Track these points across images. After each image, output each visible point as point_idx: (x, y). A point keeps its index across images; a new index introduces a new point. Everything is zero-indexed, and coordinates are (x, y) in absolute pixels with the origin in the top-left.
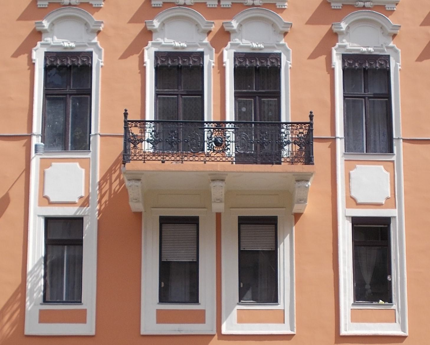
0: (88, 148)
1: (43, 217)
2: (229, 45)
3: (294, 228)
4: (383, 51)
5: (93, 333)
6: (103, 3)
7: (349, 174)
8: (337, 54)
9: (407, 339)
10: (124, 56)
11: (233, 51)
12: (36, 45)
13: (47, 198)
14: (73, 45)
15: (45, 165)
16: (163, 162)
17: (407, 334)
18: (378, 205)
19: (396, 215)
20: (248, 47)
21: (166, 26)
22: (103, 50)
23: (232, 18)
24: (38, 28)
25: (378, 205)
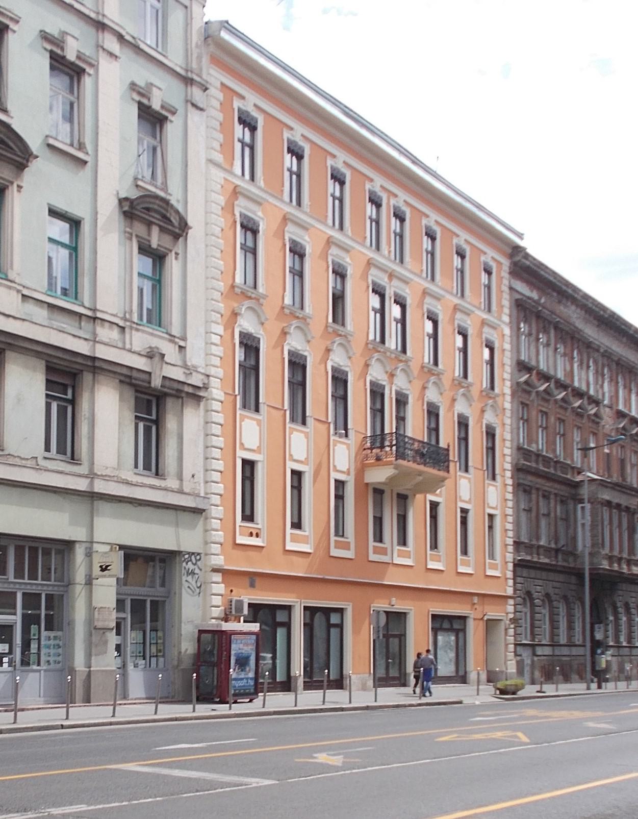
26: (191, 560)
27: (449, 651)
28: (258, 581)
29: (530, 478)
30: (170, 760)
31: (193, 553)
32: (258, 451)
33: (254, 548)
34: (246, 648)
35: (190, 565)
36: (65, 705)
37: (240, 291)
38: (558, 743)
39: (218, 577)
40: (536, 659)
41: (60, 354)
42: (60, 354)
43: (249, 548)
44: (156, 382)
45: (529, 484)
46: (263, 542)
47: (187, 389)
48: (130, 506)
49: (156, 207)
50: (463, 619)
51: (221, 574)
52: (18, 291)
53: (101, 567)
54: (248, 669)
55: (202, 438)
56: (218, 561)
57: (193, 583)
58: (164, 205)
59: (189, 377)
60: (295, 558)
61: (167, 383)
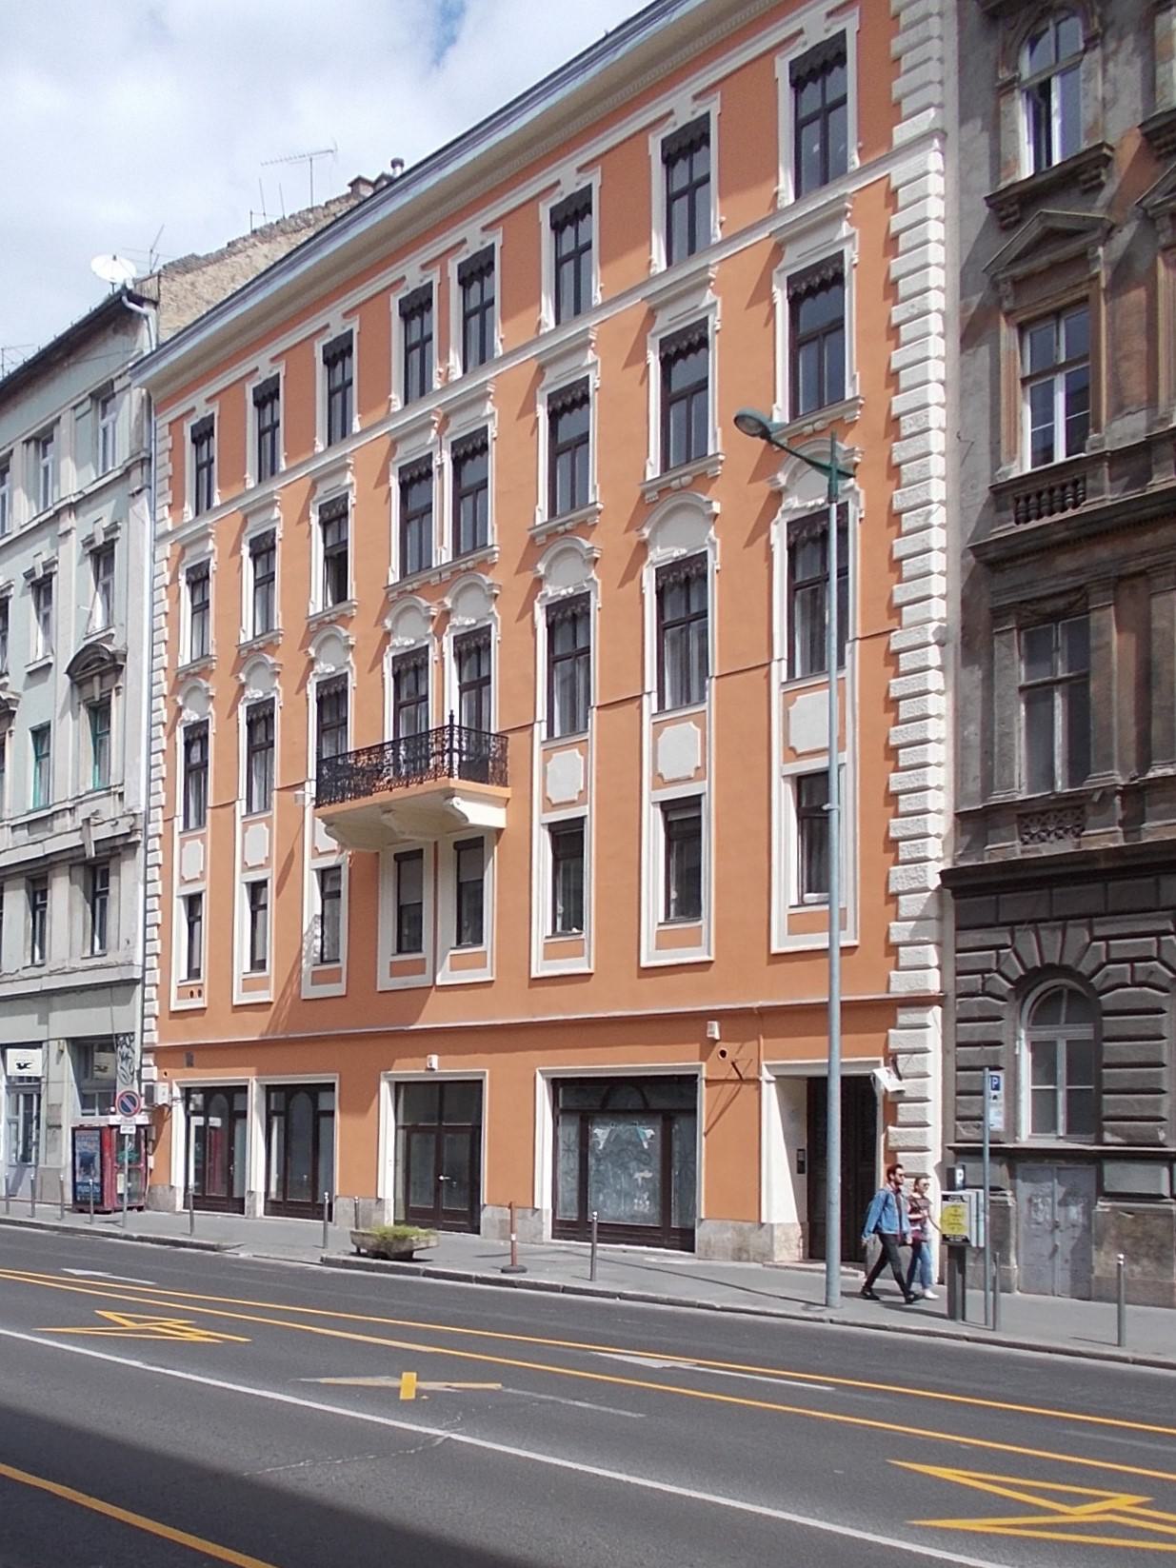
0: (76, 852)
1: (789, 779)
2: (448, 629)
3: (496, 848)
4: (583, 588)
5: (344, 993)
6: (859, 412)
7: (788, 713)
8: (541, 607)
9: (593, 977)
10: (622, 584)
11: (452, 635)
12: (775, 516)
13: (792, 749)
14: (684, 551)
15: (659, 728)
16: (421, 783)
17: (712, 958)
18: (572, 803)
19: (588, 813)
20: (804, 508)
21: (460, 600)
22: (862, 493)
23: (444, 596)
24: (776, 488)
25: (572, 803)
26: (125, 1043)
27: (633, 1164)
28: (197, 1057)
29: (1065, 562)
30: (1166, 1430)
31: (127, 1034)
32: (701, 772)
33: (784, 957)
34: (90, 1146)
35: (125, 1048)
36: (590, 1244)
37: (544, 537)
38: (323, 1380)
39: (149, 1060)
40: (1103, 1206)
41: (29, 867)
42: (29, 867)
43: (572, 978)
44: (91, 852)
45: (1069, 582)
46: (709, 954)
47: (119, 842)
48: (73, 995)
49: (92, 657)
50: (689, 1082)
51: (152, 1055)
52: (8, 825)
53: (19, 1065)
54: (93, 1172)
55: (141, 888)
56: (154, 1038)
57: (127, 1069)
58: (94, 650)
59: (117, 827)
60: (248, 1015)
61: (101, 846)
